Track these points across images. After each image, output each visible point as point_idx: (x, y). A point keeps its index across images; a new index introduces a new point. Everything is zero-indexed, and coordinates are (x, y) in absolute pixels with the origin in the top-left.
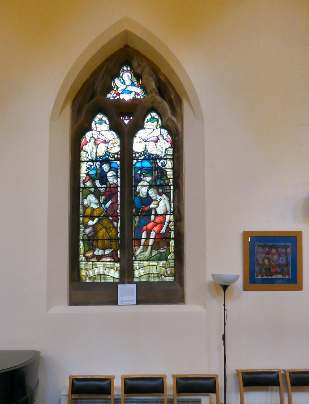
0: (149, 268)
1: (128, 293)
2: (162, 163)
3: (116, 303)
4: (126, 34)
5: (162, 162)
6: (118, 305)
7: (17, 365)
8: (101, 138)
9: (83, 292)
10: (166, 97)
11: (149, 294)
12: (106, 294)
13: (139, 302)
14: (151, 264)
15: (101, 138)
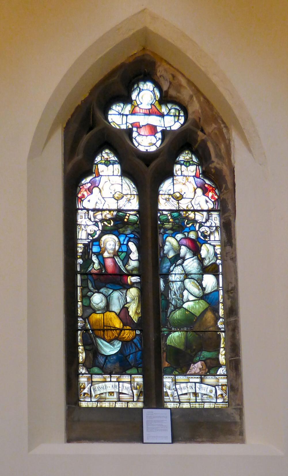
0: (202, 399)
1: (157, 424)
2: (203, 233)
3: (140, 439)
4: (145, 35)
5: (203, 230)
6: (143, 443)
7: (172, 64)
8: (110, 189)
9: (85, 425)
10: (200, 141)
11: (192, 426)
12: (124, 426)
13: (174, 439)
14: (191, 380)
15: (110, 189)
